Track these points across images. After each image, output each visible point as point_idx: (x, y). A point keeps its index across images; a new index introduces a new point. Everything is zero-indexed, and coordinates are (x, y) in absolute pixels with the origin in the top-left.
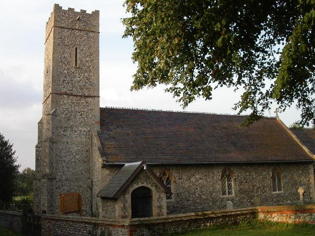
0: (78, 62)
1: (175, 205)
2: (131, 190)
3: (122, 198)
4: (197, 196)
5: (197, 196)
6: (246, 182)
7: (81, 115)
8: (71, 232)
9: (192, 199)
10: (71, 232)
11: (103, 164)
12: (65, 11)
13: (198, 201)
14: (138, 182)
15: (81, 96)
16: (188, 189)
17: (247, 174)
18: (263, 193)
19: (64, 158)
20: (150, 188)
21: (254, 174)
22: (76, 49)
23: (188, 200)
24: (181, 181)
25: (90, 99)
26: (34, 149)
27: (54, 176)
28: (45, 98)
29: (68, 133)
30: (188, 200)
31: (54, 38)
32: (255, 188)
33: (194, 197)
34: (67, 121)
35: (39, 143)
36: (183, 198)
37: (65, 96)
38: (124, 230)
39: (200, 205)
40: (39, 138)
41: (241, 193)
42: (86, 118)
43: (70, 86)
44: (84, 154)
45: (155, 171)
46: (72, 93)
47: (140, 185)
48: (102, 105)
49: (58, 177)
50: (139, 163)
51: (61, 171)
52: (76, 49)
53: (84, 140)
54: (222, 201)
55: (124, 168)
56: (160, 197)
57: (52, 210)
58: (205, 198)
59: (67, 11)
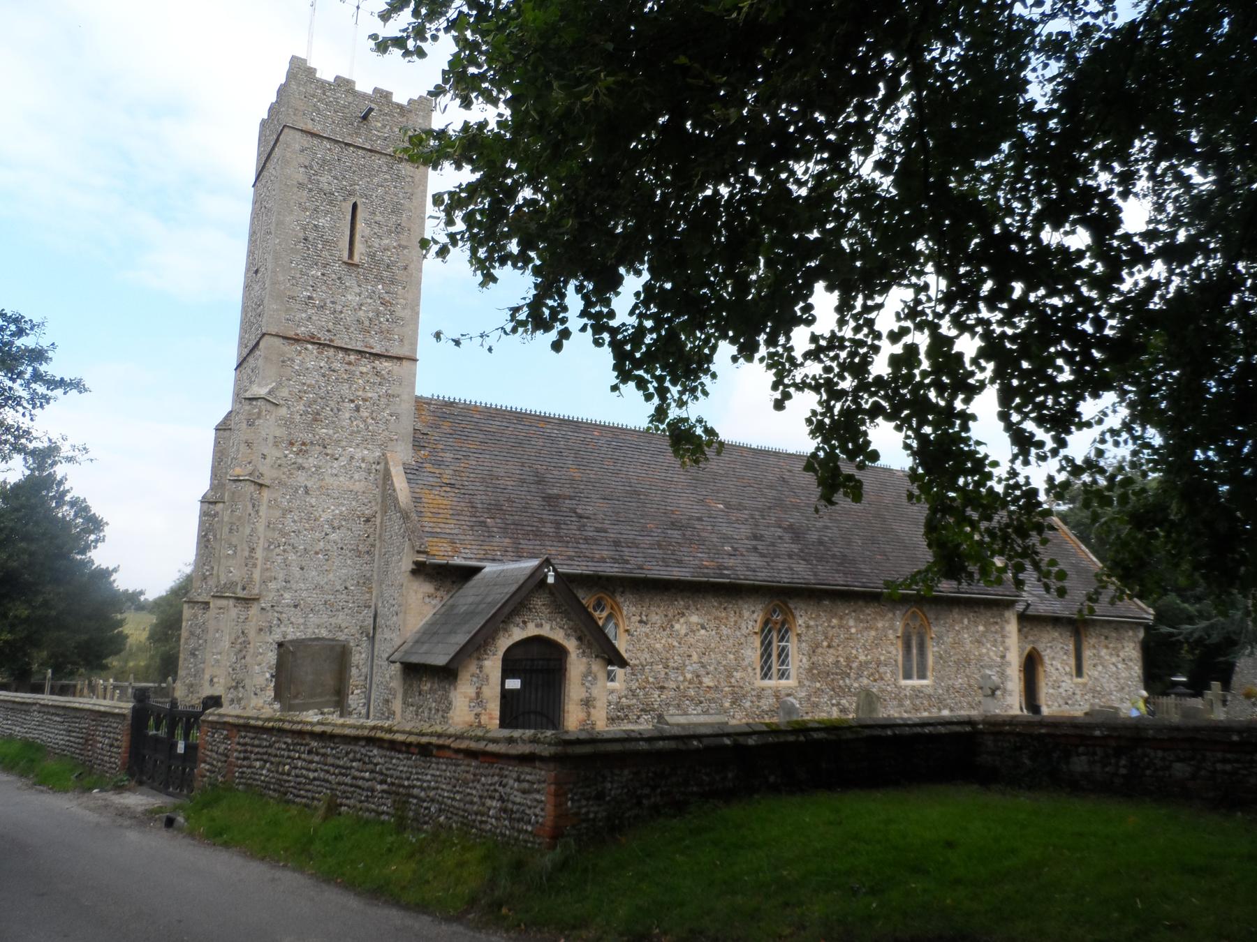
0: (359, 247)
1: (624, 700)
2: (504, 643)
3: (473, 668)
4: (689, 676)
5: (689, 676)
6: (829, 646)
7: (357, 409)
8: (311, 775)
9: (673, 685)
10: (311, 775)
11: (416, 563)
12: (323, 84)
13: (692, 693)
14: (525, 622)
15: (360, 352)
16: (664, 654)
17: (835, 621)
18: (875, 681)
19: (293, 539)
20: (561, 641)
21: (851, 623)
22: (355, 206)
23: (662, 688)
24: (646, 629)
25: (387, 364)
26: (196, 509)
27: (256, 591)
28: (246, 351)
29: (311, 462)
30: (662, 688)
31: (179, 637)
32: (854, 665)
33: (681, 678)
34: (310, 425)
35: (213, 487)
36: (648, 682)
37: (310, 347)
38: (532, 774)
39: (697, 705)
40: (214, 475)
41: (813, 678)
42: (370, 421)
43: (325, 320)
44: (359, 528)
45: (580, 594)
46: (331, 341)
47: (532, 631)
48: (418, 392)
49: (271, 596)
50: (534, 563)
51: (281, 576)
52: (355, 206)
53: (359, 487)
54: (759, 697)
55: (479, 576)
56: (589, 672)
57: (240, 700)
58: (711, 684)
59: (330, 84)
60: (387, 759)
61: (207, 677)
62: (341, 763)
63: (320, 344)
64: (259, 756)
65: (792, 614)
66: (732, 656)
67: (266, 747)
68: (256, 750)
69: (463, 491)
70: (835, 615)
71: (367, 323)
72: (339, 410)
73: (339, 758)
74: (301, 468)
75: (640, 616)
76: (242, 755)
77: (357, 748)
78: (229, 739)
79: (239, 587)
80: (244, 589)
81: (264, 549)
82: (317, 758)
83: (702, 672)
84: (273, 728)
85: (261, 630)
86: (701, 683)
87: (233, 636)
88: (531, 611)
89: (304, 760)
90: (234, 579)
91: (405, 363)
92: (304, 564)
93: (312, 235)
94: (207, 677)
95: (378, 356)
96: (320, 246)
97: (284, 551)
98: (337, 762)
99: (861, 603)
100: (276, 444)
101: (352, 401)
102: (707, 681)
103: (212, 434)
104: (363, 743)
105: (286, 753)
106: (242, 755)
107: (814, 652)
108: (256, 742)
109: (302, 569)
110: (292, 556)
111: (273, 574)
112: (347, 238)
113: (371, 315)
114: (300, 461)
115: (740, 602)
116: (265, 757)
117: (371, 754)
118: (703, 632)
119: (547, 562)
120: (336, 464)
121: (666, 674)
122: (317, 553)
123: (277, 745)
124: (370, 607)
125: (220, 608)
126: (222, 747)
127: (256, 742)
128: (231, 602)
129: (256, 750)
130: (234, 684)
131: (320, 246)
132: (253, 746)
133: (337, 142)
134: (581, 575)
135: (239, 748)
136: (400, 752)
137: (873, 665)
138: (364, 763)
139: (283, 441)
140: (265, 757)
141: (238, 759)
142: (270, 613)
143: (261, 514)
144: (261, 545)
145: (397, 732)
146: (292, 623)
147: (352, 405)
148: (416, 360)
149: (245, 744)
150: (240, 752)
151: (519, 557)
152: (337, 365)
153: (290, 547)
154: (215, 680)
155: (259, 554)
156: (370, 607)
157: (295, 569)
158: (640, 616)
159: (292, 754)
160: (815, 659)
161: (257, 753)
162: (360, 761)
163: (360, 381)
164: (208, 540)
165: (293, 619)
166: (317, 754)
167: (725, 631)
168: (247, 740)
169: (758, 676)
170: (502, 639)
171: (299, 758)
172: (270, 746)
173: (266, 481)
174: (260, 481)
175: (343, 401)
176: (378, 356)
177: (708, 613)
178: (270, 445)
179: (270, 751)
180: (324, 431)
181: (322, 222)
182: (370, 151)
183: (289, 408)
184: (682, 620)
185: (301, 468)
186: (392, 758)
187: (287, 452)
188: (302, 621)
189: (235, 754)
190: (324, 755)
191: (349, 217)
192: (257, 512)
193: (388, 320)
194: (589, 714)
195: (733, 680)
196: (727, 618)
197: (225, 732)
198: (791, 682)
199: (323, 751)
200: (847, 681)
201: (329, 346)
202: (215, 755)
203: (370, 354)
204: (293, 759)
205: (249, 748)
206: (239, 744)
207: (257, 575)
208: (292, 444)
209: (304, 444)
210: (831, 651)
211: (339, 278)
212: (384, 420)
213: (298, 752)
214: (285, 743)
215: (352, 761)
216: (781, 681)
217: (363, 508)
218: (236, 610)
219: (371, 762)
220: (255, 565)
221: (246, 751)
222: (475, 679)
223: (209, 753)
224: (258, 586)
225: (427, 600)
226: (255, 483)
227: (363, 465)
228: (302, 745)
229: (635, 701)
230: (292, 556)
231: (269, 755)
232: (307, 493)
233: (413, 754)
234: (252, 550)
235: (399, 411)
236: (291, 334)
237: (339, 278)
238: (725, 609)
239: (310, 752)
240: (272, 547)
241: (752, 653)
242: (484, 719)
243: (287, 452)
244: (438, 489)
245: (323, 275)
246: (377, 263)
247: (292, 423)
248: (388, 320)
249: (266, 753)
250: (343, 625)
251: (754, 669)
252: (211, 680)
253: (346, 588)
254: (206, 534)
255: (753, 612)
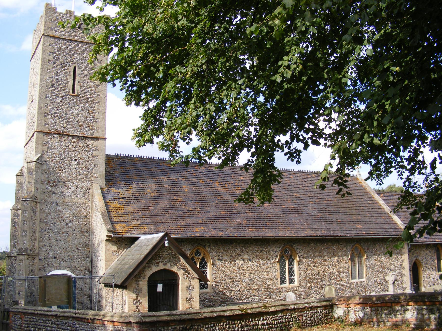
0: (77, 87)
1: (212, 297)
2: (148, 273)
6: (314, 266)
7: (79, 164)
13: (246, 292)
14: (158, 263)
15: (79, 136)
22: (75, 68)
25: (92, 142)
27: (37, 252)
37: (56, 136)
41: (307, 281)
46: (66, 132)
47: (161, 267)
48: (108, 153)
49: (43, 254)
51: (47, 244)
52: (75, 68)
60: (81, 326)
61: (17, 292)
62: (64, 328)
63: (60, 134)
64: (33, 326)
65: (295, 251)
66: (265, 274)
67: (35, 322)
68: (32, 323)
69: (129, 201)
70: (317, 251)
71: (82, 123)
72: (70, 165)
73: (63, 326)
74: (54, 193)
75: (219, 257)
76: (26, 326)
77: (69, 322)
78: (21, 319)
79: (29, 250)
80: (31, 251)
81: (39, 232)
82: (54, 326)
83: (251, 282)
84: (37, 314)
85: (40, 269)
86: (250, 287)
87: (28, 272)
88: (160, 258)
89: (50, 327)
90: (26, 246)
91: (100, 141)
92: (57, 238)
93: (56, 84)
94: (17, 292)
95: (87, 138)
96: (59, 88)
97: (48, 232)
98: (62, 327)
99: (330, 244)
100: (42, 183)
101: (76, 160)
102: (253, 286)
103: (15, 178)
104: (71, 319)
105: (43, 324)
106: (26, 326)
107: (307, 269)
108: (32, 320)
109: (57, 240)
110: (52, 235)
111: (44, 244)
112: (71, 83)
113: (83, 118)
114: (53, 190)
115: (269, 247)
116: (35, 326)
117: (74, 323)
118: (250, 263)
119: (166, 235)
120: (70, 190)
121: (233, 284)
122: (63, 233)
123: (39, 321)
124: (89, 257)
125: (21, 260)
126: (19, 322)
127: (32, 320)
128: (26, 257)
129: (32, 323)
130: (29, 295)
131: (59, 88)
132: (30, 321)
133: (66, 40)
134: (188, 238)
135: (25, 322)
136: (85, 322)
137: (337, 274)
138: (72, 327)
139: (45, 181)
140: (35, 326)
141: (25, 327)
142: (44, 262)
143: (37, 216)
144: (38, 229)
145: (83, 314)
146: (53, 266)
147: (76, 162)
148: (105, 139)
149: (27, 321)
150: (26, 324)
151: (157, 232)
152: (68, 144)
153: (51, 231)
154: (21, 293)
155: (37, 234)
156: (89, 257)
157: (53, 241)
158: (219, 257)
159: (45, 324)
160: (307, 273)
161: (32, 324)
162: (70, 326)
163: (79, 150)
164: (16, 228)
165: (54, 264)
166: (55, 324)
167: (261, 262)
168: (28, 319)
169: (279, 283)
170: (148, 271)
171: (48, 326)
172: (37, 321)
173: (39, 200)
174: (36, 201)
175: (72, 160)
176: (87, 138)
177: (253, 253)
178: (40, 183)
179: (37, 323)
180: (64, 175)
181: (59, 77)
182: (82, 42)
183: (47, 165)
184: (240, 258)
185: (54, 193)
186: (82, 325)
187: (47, 186)
188: (58, 265)
189: (24, 325)
190: (57, 324)
191: (72, 74)
192: (35, 215)
193: (91, 121)
194: (191, 305)
195: (266, 285)
196: (262, 256)
197: (20, 316)
198: (364, 279)
199: (57, 323)
200: (324, 282)
201: (65, 135)
202: (16, 326)
203: (84, 137)
204: (46, 326)
205: (29, 322)
206: (25, 321)
207: (37, 245)
208: (49, 182)
209: (55, 182)
210: (315, 268)
211: (69, 103)
212: (91, 168)
213: (47, 323)
214: (43, 320)
215: (68, 326)
216: (291, 285)
217: (83, 210)
218: (28, 260)
219: (74, 327)
220: (36, 240)
221: (28, 324)
222: (135, 290)
223: (13, 325)
224: (37, 249)
225: (114, 253)
226: (34, 201)
227: (82, 190)
228: (49, 320)
229: (217, 298)
230: (52, 235)
231: (37, 325)
232: (57, 205)
233: (90, 323)
234: (34, 233)
235: (98, 164)
236: (47, 131)
237: (69, 103)
238: (261, 251)
239: (52, 323)
240: (43, 231)
241: (276, 272)
242: (141, 308)
243: (47, 186)
244: (118, 200)
245: (61, 102)
246: (85, 93)
247: (49, 172)
248: (91, 121)
249: (35, 324)
250: (77, 267)
251: (277, 279)
252: (19, 293)
253: (77, 249)
254: (14, 225)
255: (276, 252)
